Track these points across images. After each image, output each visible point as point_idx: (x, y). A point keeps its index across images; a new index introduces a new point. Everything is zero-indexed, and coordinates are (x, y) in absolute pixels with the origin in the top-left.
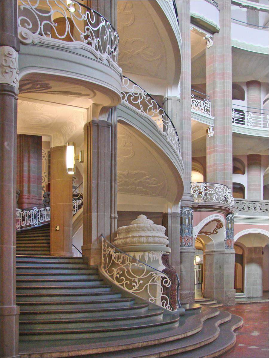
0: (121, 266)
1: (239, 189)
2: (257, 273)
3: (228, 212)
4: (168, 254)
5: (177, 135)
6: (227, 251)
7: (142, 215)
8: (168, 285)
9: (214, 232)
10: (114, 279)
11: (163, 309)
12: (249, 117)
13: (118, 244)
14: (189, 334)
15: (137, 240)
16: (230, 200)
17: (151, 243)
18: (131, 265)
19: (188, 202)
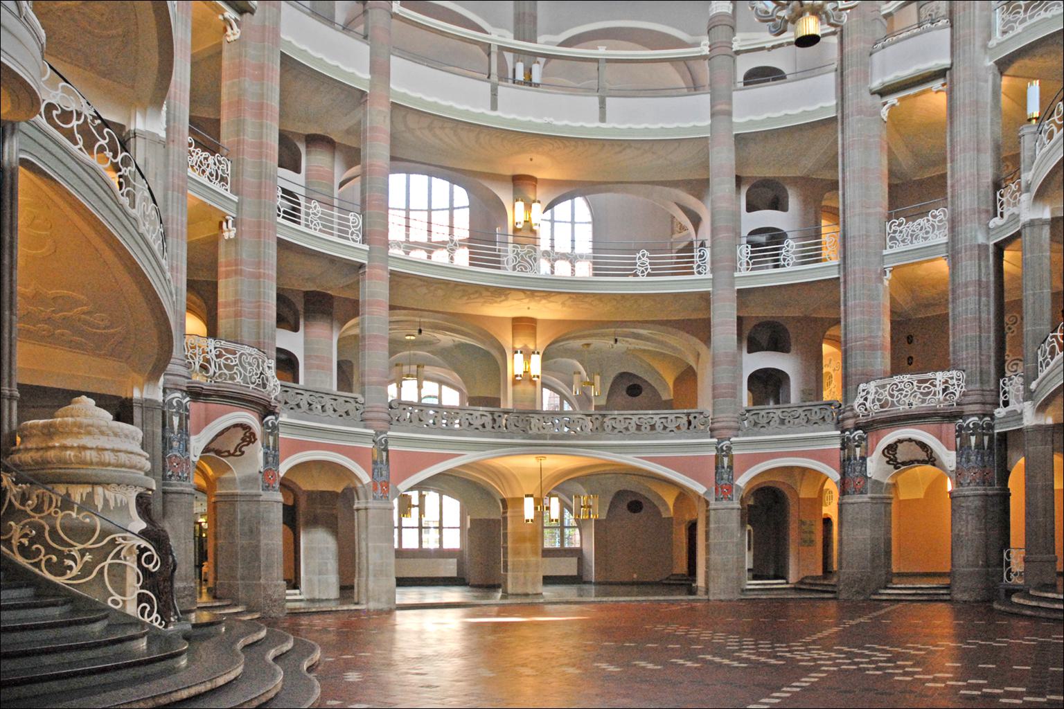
0: (34, 517)
1: (287, 364)
2: (327, 548)
3: (266, 410)
4: (150, 492)
5: (161, 223)
6: (266, 496)
7: (84, 397)
8: (154, 567)
9: (235, 451)
10: (13, 552)
11: (143, 624)
12: (313, 210)
13: (21, 461)
14: (221, 681)
15: (75, 456)
16: (272, 385)
17: (109, 464)
18: (60, 514)
19: (178, 378)
